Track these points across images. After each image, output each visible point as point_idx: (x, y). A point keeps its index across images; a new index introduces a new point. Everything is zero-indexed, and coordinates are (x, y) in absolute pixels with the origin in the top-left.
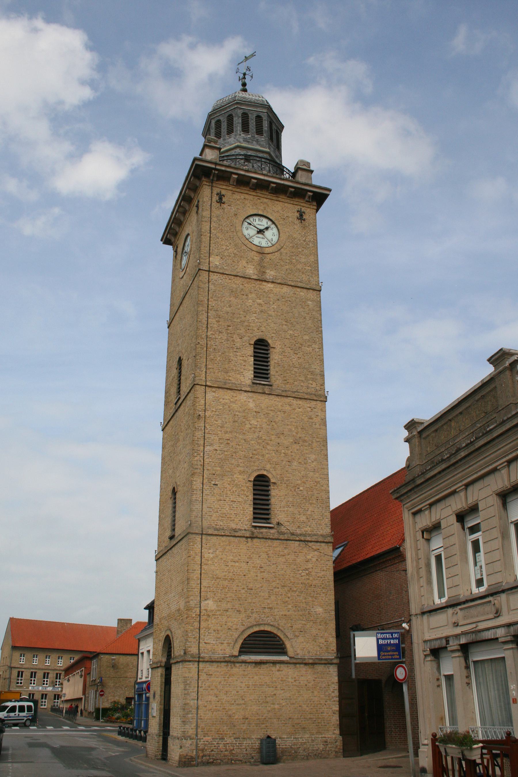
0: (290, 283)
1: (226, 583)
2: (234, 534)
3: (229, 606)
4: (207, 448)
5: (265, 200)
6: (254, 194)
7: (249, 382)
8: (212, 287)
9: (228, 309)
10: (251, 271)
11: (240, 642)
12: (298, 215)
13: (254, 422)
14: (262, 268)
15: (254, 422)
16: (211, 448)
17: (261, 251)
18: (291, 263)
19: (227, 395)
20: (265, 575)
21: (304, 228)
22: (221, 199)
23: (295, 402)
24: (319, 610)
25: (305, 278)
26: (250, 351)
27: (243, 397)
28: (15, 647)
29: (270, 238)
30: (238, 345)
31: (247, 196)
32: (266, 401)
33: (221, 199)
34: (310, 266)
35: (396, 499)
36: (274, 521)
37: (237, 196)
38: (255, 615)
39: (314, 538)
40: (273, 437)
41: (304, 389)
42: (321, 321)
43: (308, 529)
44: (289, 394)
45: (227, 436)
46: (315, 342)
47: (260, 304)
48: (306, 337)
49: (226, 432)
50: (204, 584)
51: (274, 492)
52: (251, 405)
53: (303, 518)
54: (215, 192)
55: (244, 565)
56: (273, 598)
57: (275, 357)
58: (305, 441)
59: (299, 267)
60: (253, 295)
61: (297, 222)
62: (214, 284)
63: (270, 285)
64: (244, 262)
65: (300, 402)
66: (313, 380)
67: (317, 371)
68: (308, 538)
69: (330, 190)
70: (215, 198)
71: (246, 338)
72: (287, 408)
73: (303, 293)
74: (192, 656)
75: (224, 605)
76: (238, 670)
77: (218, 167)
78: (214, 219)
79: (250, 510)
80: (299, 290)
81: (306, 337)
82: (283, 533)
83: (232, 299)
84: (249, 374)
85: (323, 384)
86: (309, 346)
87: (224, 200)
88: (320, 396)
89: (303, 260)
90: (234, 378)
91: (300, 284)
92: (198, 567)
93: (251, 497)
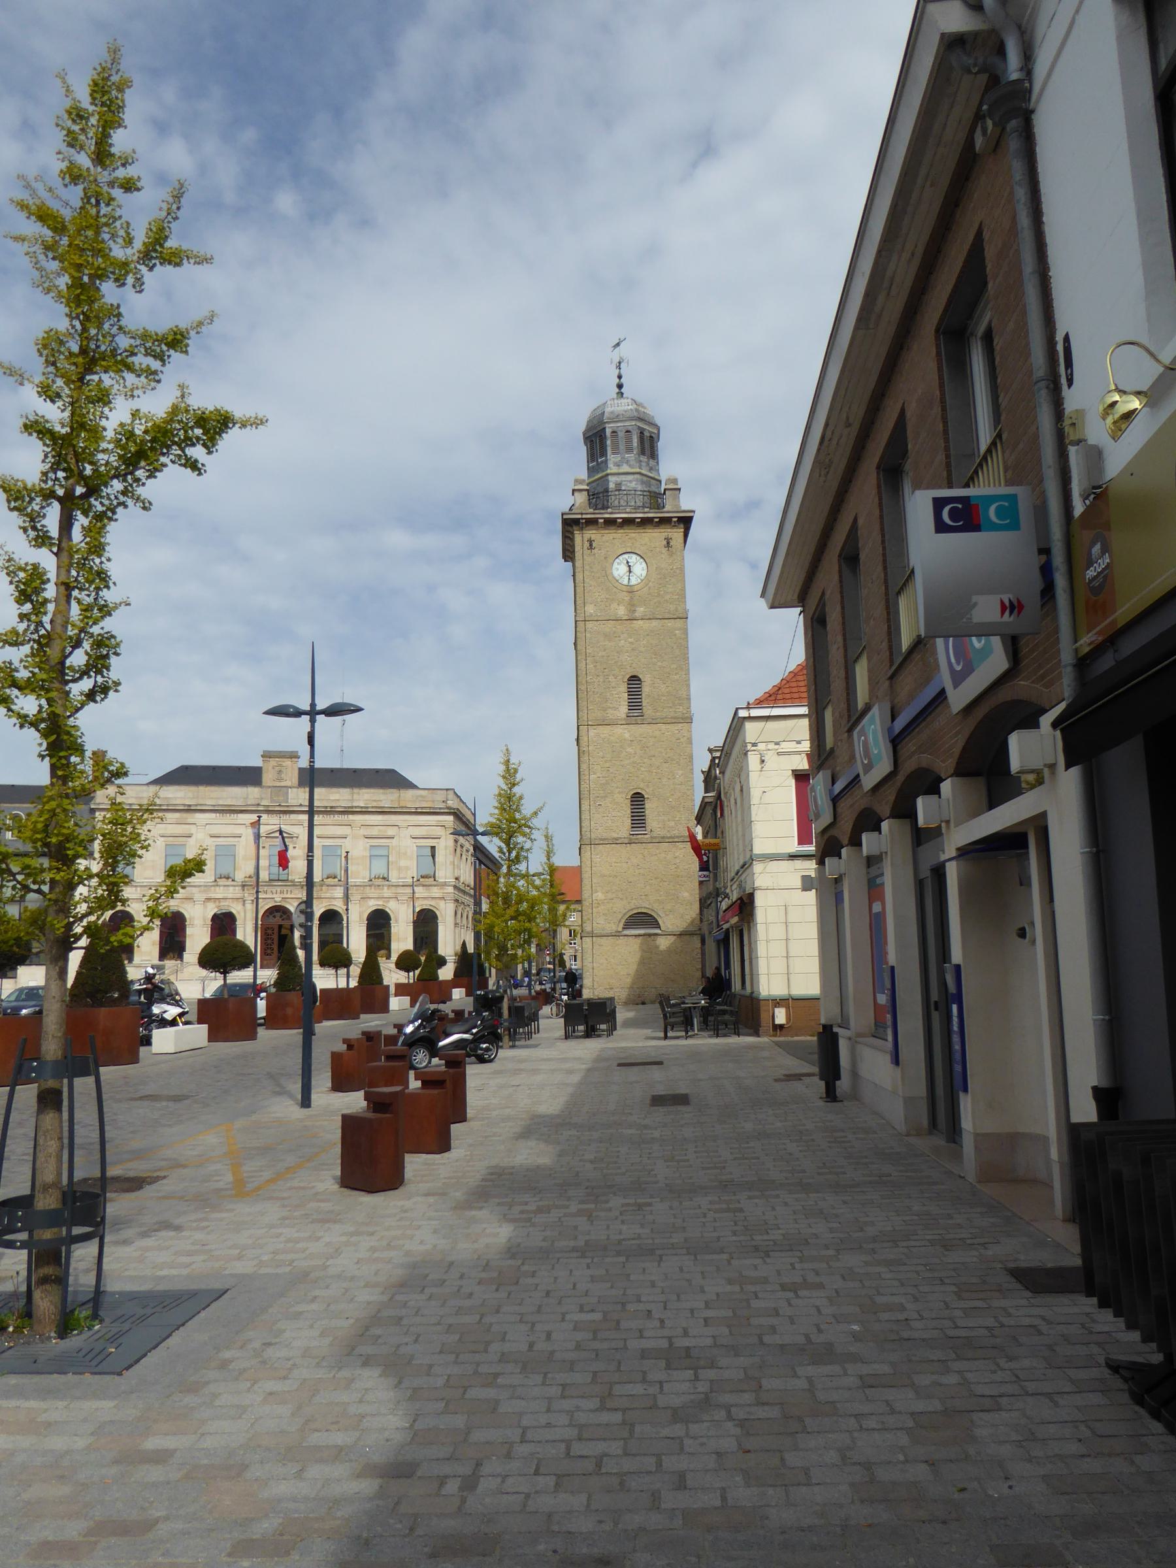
0: (658, 617)
1: (611, 879)
2: (616, 842)
3: (614, 895)
4: (592, 777)
5: (634, 535)
6: (622, 531)
7: (624, 716)
8: (588, 635)
9: (604, 653)
10: (622, 611)
11: (623, 921)
12: (665, 542)
13: (629, 750)
14: (632, 607)
15: (629, 750)
16: (595, 776)
17: (630, 590)
18: (659, 595)
19: (605, 731)
20: (642, 871)
21: (671, 555)
22: (591, 545)
23: (663, 726)
24: (686, 894)
25: (672, 607)
26: (623, 688)
27: (619, 730)
28: (948, 483)
29: (639, 574)
30: (613, 684)
31: (615, 535)
33: (591, 545)
34: (678, 594)
35: (563, 894)
36: (648, 828)
37: (606, 537)
38: (634, 901)
39: (681, 840)
40: (645, 760)
41: (672, 714)
42: (687, 647)
43: (676, 832)
44: (658, 721)
45: (607, 765)
46: (682, 669)
47: (631, 643)
48: (674, 666)
49: (606, 761)
50: (594, 881)
51: (648, 805)
52: (627, 735)
53: (672, 824)
54: (585, 539)
55: (625, 865)
56: (648, 887)
57: (646, 689)
58: (673, 760)
59: (668, 597)
60: (625, 635)
61: (664, 550)
62: (590, 632)
63: (640, 622)
64: (614, 605)
65: (668, 726)
66: (680, 704)
67: (684, 696)
68: (676, 840)
69: (694, 512)
70: (587, 544)
71: (620, 677)
72: (657, 733)
73: (670, 623)
74: (588, 933)
75: (610, 895)
76: (622, 940)
77: (584, 516)
78: (587, 567)
79: (628, 822)
80: (666, 621)
81: (674, 666)
82: (655, 838)
83: (607, 643)
84: (624, 709)
85: (689, 707)
86: (676, 674)
87: (594, 545)
88: (687, 718)
89: (670, 590)
90: (611, 714)
92: (589, 869)
93: (629, 811)
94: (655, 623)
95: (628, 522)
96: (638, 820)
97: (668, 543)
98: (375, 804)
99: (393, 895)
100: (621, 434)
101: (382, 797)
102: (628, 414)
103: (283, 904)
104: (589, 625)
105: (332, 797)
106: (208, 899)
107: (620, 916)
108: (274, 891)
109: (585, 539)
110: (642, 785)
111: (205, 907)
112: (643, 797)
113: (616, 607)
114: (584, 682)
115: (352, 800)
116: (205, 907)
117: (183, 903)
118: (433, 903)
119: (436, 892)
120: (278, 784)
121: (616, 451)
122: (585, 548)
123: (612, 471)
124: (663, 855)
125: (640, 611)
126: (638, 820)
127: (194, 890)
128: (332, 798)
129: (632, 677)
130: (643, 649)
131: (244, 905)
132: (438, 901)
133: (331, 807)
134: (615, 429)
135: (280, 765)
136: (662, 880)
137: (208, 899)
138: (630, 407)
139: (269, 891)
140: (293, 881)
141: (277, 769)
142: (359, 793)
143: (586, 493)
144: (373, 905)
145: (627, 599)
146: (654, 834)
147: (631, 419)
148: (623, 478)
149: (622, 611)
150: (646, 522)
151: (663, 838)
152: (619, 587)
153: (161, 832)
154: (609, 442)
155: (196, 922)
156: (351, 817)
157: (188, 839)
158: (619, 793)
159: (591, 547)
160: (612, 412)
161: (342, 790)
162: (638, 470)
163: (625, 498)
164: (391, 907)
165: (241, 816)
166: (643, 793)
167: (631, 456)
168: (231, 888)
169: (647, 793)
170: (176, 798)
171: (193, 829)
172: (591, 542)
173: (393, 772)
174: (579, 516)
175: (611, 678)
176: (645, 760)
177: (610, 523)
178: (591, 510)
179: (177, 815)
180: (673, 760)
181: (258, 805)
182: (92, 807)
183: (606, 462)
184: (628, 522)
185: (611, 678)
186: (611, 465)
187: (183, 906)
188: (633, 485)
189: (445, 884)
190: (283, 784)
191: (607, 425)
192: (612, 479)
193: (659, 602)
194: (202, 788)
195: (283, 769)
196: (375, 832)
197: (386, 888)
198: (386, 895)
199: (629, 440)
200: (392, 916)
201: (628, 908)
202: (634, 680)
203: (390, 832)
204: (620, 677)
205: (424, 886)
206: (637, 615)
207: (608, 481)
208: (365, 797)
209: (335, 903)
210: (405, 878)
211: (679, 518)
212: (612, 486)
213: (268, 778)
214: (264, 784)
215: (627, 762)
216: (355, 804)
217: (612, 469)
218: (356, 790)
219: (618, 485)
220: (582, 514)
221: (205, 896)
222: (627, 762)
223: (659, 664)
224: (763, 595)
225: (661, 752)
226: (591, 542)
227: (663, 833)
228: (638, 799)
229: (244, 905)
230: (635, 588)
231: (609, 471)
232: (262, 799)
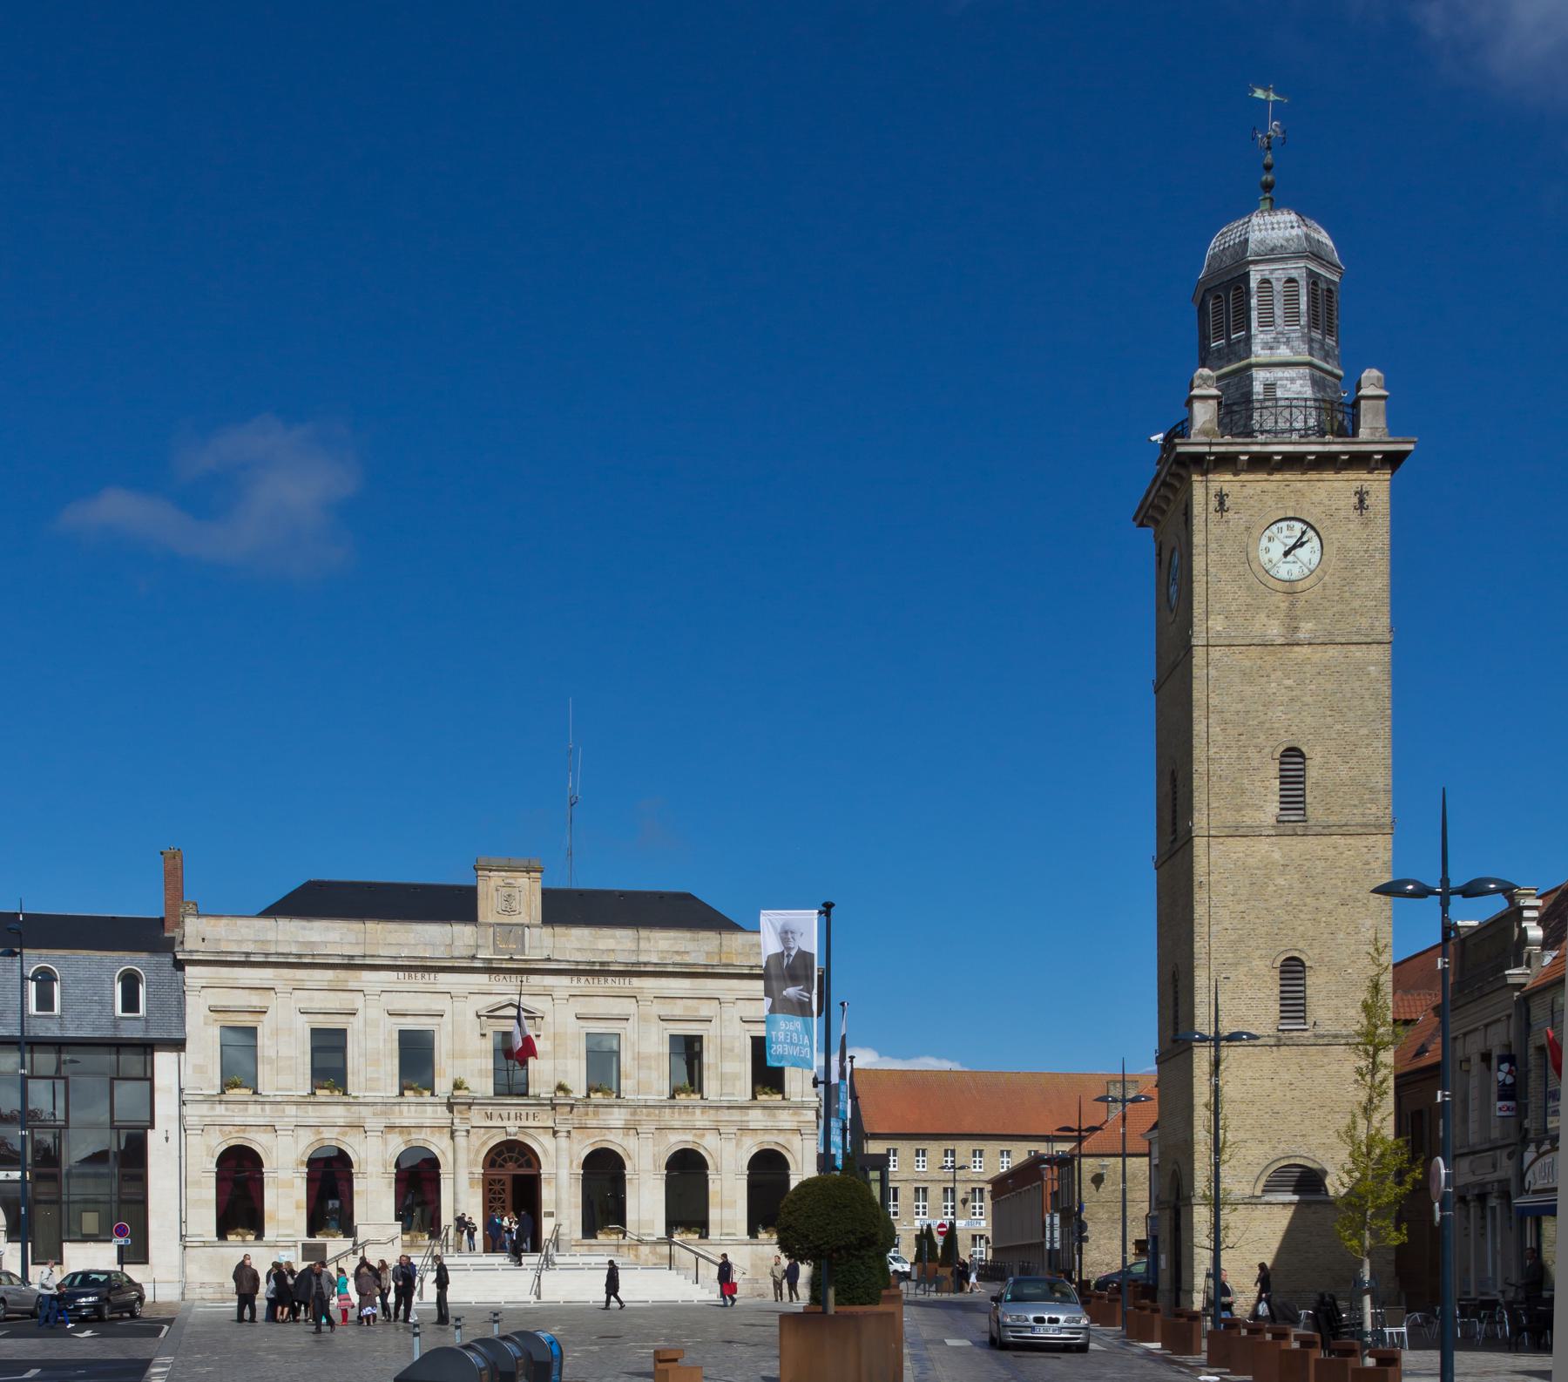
0: (1339, 639)
3: (1248, 1135)
4: (1213, 929)
5: (1299, 485)
7: (1273, 821)
8: (1213, 672)
9: (1240, 706)
10: (1275, 631)
12: (1355, 500)
16: (1220, 927)
17: (1291, 589)
18: (1342, 600)
19: (1238, 846)
20: (1297, 1093)
22: (1221, 503)
23: (1341, 841)
26: (1273, 769)
27: (1263, 846)
29: (1306, 560)
30: (1255, 763)
32: (1298, 846)
33: (1221, 503)
36: (1310, 1021)
38: (1282, 1145)
40: (1308, 900)
41: (1359, 820)
45: (1242, 907)
47: (1289, 688)
48: (1364, 731)
52: (1277, 856)
54: (1212, 492)
55: (1268, 1083)
56: (1307, 1122)
57: (1313, 774)
58: (1357, 900)
59: (1356, 604)
60: (1279, 673)
61: (1355, 515)
63: (1306, 650)
65: (1350, 840)
66: (1372, 801)
70: (1214, 503)
71: (1267, 750)
72: (1331, 853)
73: (1358, 653)
76: (1261, 1212)
77: (1215, 449)
78: (1213, 546)
80: (1353, 648)
81: (1364, 731)
82: (1323, 1036)
84: (1273, 808)
89: (1363, 590)
90: (1250, 818)
91: (1355, 639)
93: (1277, 990)
94: (1332, 651)
95: (1293, 462)
96: (1293, 1004)
97: (1361, 501)
98: (678, 959)
99: (794, 1125)
100: (1278, 286)
101: (690, 946)
102: (1293, 246)
103: (520, 1138)
104: (1215, 653)
105: (602, 945)
106: (391, 1128)
107: (1258, 1170)
108: (505, 1115)
109: (1212, 492)
110: (1301, 945)
111: (386, 1143)
112: (1303, 965)
113: (1265, 620)
114: (1203, 758)
115: (638, 951)
116: (386, 1143)
117: (344, 1134)
118: (781, 1139)
119: (786, 1119)
120: (506, 920)
121: (1267, 323)
122: (1211, 509)
123: (1261, 360)
124: (1336, 1067)
125: (1306, 629)
126: (1293, 1004)
127: (364, 1111)
128: (601, 947)
129: (1289, 749)
130: (1307, 699)
131: (452, 1137)
132: (789, 1135)
133: (602, 964)
134: (1267, 275)
135: (509, 885)
136: (1332, 1111)
137: (391, 1128)
138: (1295, 232)
139: (495, 1114)
140: (537, 1097)
141: (505, 891)
142: (649, 939)
143: (1213, 403)
144: (676, 1141)
145: (1284, 605)
146: (1321, 1031)
147: (1298, 255)
148: (1279, 373)
149: (1275, 631)
150: (1326, 462)
151: (1336, 1036)
152: (1272, 583)
153: (304, 1005)
154: (1254, 302)
155: (370, 1169)
156: (636, 982)
157: (351, 1018)
158: (1261, 957)
159: (1222, 507)
160: (1262, 242)
161: (620, 933)
162: (1307, 358)
163: (1286, 413)
164: (709, 1145)
165: (441, 976)
166: (1303, 957)
167: (1295, 332)
168: (429, 1109)
169: (1309, 959)
170: (325, 943)
171: (357, 1001)
172: (1221, 497)
173: (688, 897)
174: (1206, 449)
175: (1252, 752)
176: (1308, 900)
177: (1260, 462)
178: (1228, 438)
179: (329, 974)
180: (1357, 900)
181: (474, 957)
182: (180, 956)
183: (1248, 340)
184: (1293, 462)
185: (1252, 752)
186: (1257, 348)
187: (346, 1139)
188: (1297, 386)
189: (801, 1107)
190: (515, 920)
191: (1252, 267)
192: (1260, 377)
193: (1342, 613)
194: (371, 926)
195: (515, 892)
196: (678, 1009)
197: (698, 1111)
198: (699, 1124)
199: (1292, 299)
200: (710, 1162)
201: (1273, 1156)
202: (1293, 754)
203: (706, 1009)
204: (1267, 750)
205: (765, 1108)
206: (1301, 636)
207: (1250, 379)
208: (661, 944)
209: (611, 1137)
210: (733, 1094)
211: (1386, 454)
212: (1258, 387)
213: (488, 908)
214: (481, 919)
215: (1276, 902)
216: (643, 959)
217: (1259, 353)
218: (644, 933)
219: (1270, 387)
220: (1210, 444)
221: (383, 1122)
222: (1276, 902)
223: (1339, 727)
224: (1134, 520)
225: (1335, 886)
226: (1221, 497)
227: (1333, 1028)
228: (1293, 969)
229: (452, 1137)
230: (1300, 586)
231: (1253, 360)
232: (478, 947)
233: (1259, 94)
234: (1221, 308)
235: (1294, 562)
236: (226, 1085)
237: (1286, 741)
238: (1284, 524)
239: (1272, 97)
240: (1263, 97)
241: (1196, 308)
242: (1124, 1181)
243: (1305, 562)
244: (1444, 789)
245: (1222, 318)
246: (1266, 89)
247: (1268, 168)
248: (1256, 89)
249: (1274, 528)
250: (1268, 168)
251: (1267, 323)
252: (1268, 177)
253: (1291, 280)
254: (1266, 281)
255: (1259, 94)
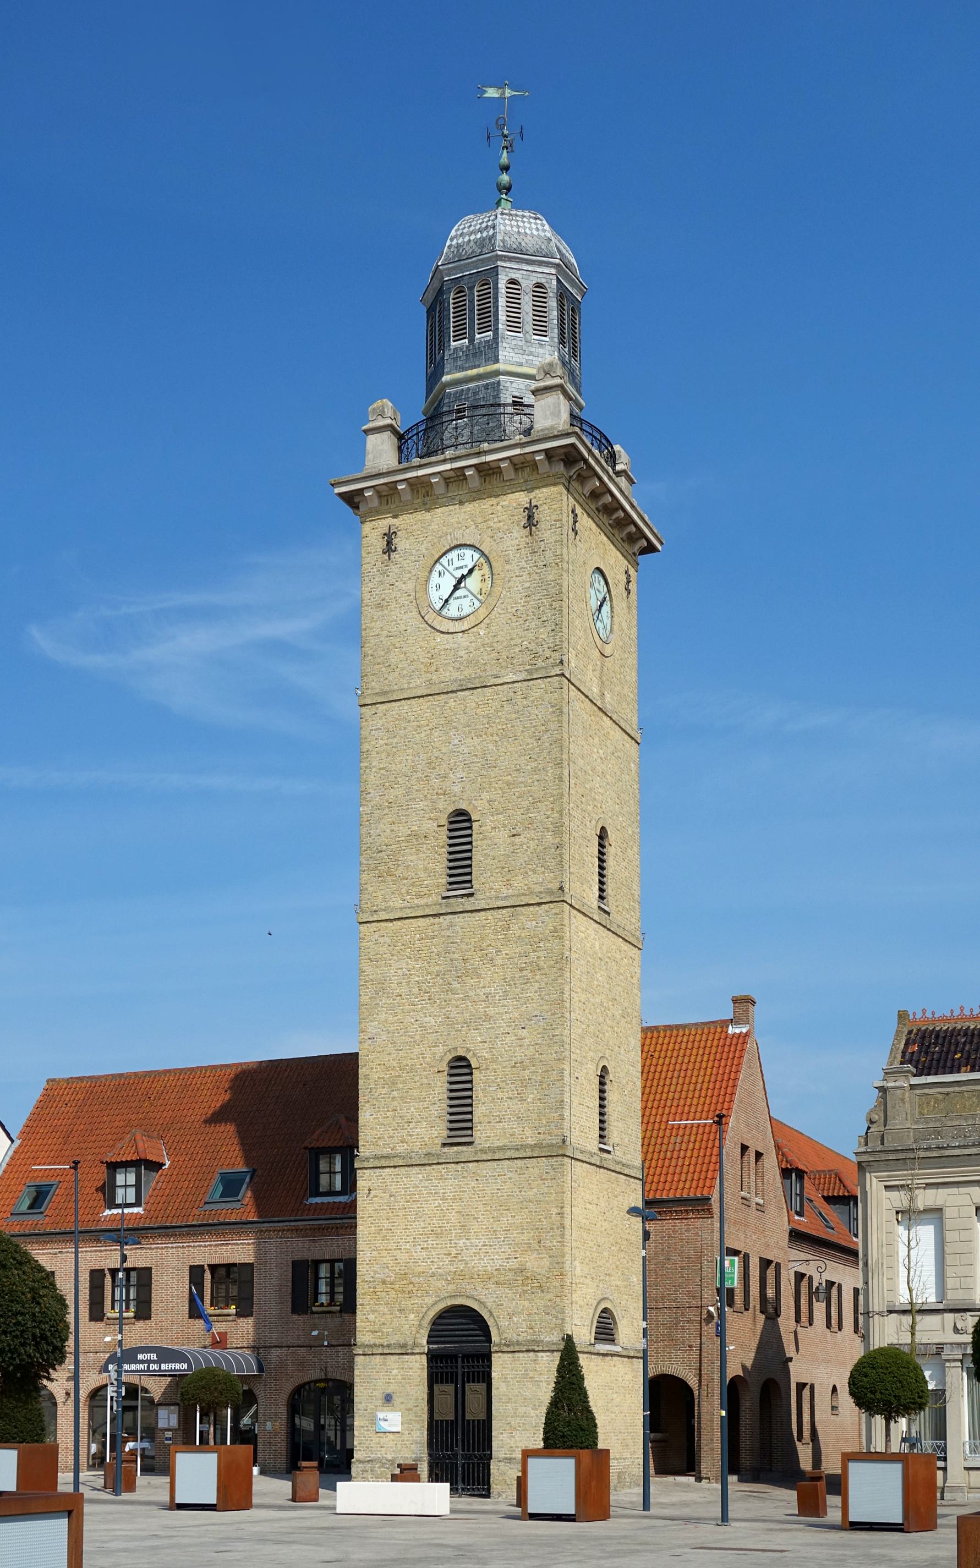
91: (622, 724)
231: (501, 366)
233: (492, 93)
234: (464, 298)
235: (464, 597)
236: (490, 347)
237: (441, 1055)
238: (453, 555)
239: (508, 93)
240: (496, 95)
241: (424, 310)
242: (282, 1347)
243: (476, 593)
244: (603, 835)
245: (465, 309)
246: (500, 86)
247: (505, 169)
248: (487, 89)
249: (444, 561)
250: (505, 169)
251: (515, 324)
252: (505, 178)
253: (539, 285)
254: (513, 281)
255: (492, 93)
